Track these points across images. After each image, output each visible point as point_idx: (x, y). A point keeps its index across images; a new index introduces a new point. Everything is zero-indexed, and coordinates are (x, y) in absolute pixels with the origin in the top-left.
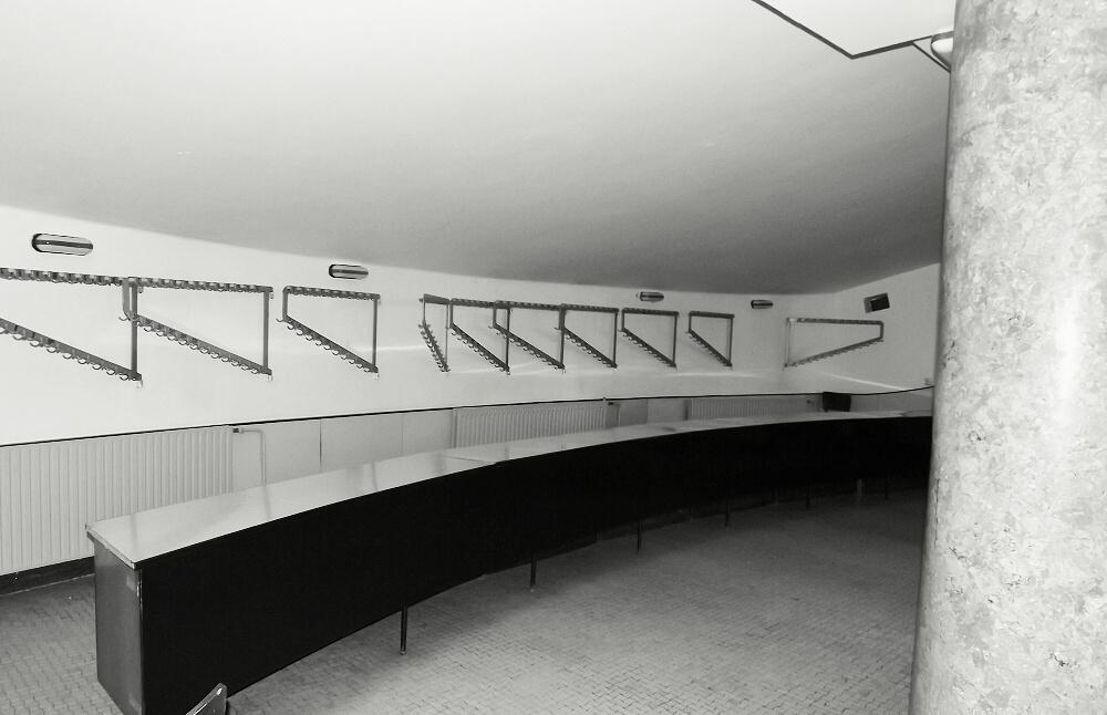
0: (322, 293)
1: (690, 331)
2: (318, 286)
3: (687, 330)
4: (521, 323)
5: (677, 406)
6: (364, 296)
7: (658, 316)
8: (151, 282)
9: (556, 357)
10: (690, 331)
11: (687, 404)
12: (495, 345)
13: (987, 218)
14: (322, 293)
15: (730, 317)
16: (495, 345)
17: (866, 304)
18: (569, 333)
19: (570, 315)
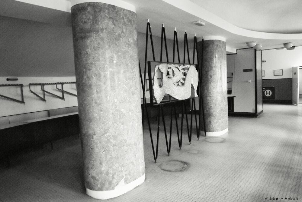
0: (6, 85)
1: (30, 91)
2: (4, 84)
3: (29, 90)
4: (66, 88)
5: (46, 113)
6: (17, 85)
7: (254, 77)
8: (65, 83)
9: (61, 96)
10: (30, 91)
11: (49, 113)
12: (60, 94)
13: (118, 158)
14: (6, 85)
15: (283, 75)
16: (60, 94)
17: (243, 70)
18: (46, 91)
19: (65, 85)
